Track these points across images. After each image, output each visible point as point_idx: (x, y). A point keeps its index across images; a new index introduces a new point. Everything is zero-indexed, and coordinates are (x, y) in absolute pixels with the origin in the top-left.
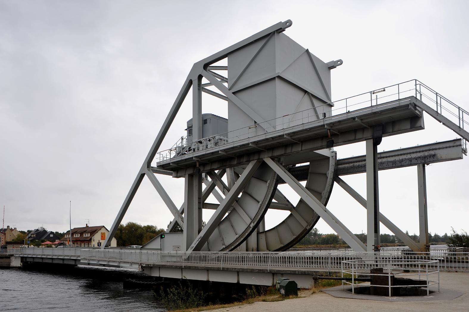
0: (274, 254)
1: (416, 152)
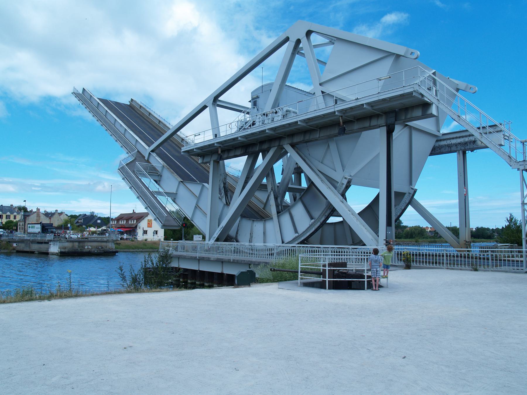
0: (337, 249)
1: (456, 138)
